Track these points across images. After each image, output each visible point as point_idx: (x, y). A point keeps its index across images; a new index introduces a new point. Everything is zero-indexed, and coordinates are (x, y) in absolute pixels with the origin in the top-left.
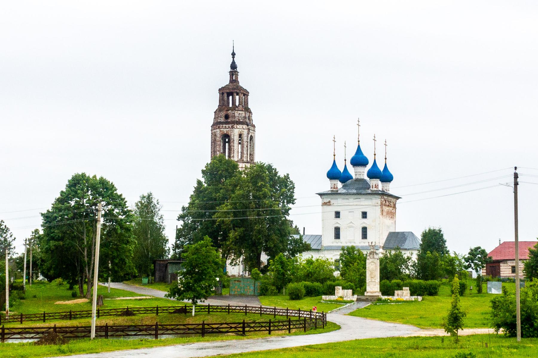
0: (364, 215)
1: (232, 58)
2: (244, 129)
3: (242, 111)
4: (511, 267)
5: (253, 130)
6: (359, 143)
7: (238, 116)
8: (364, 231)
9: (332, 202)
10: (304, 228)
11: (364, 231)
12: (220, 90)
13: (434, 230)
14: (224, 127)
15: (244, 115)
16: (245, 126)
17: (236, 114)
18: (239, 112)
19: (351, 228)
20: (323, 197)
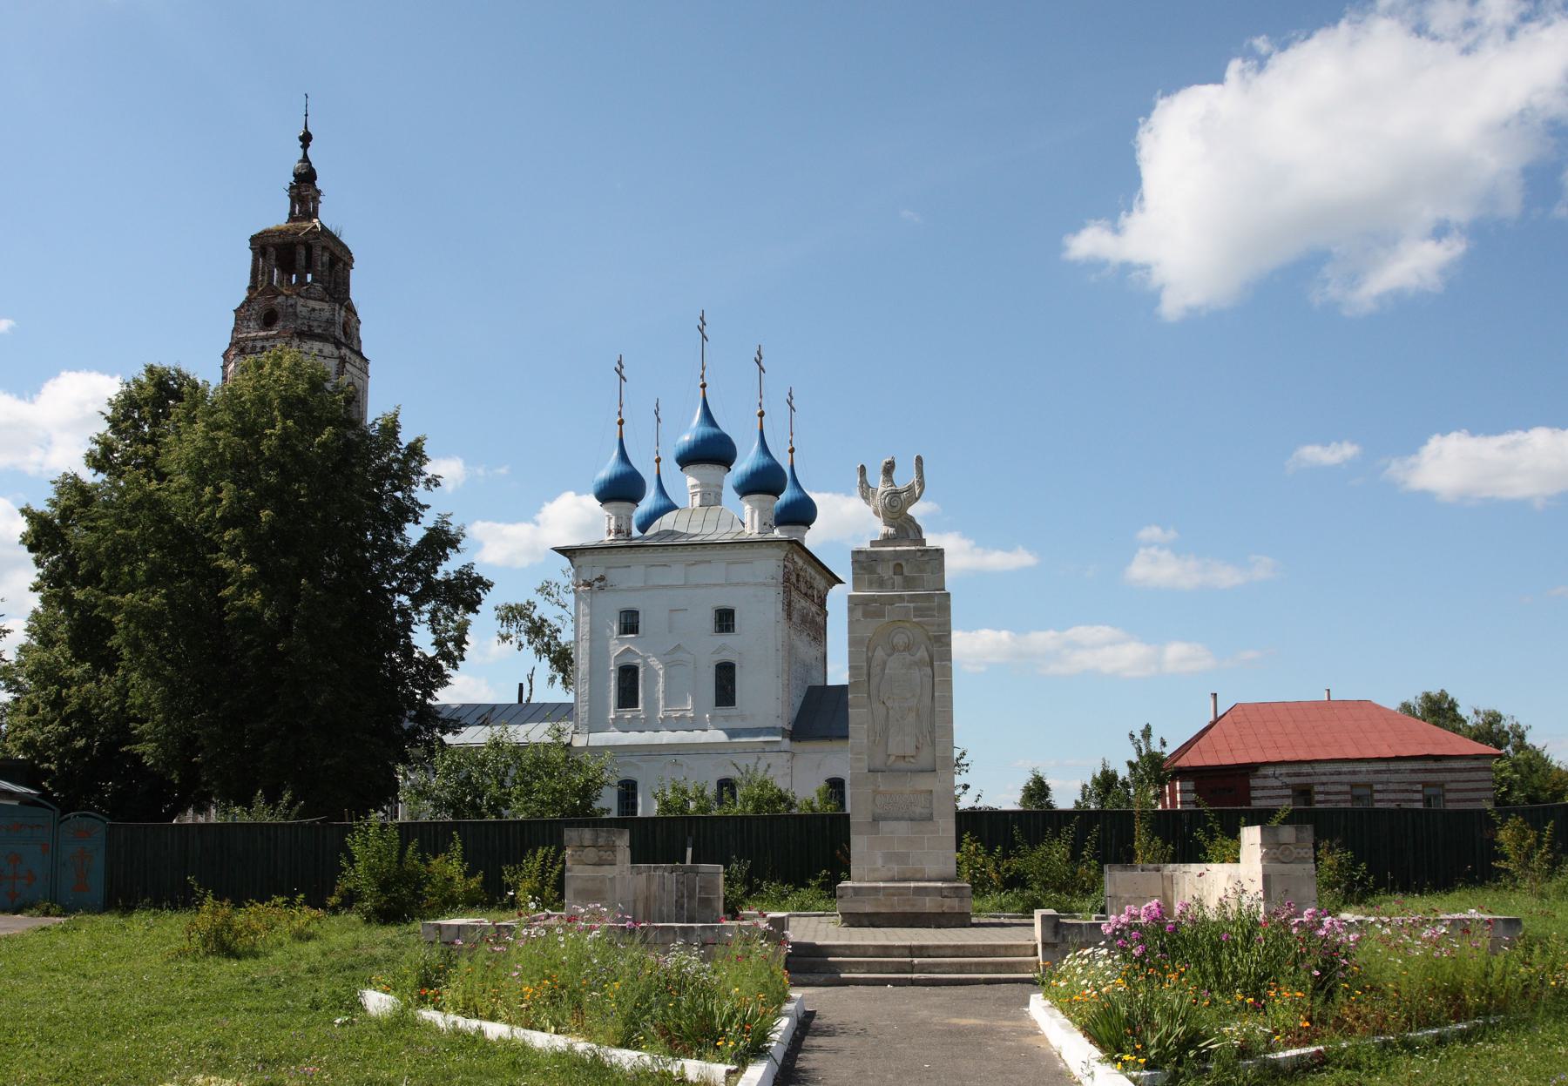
0: (725, 620)
2: (325, 357)
3: (322, 300)
4: (1289, 792)
5: (361, 369)
7: (307, 315)
9: (614, 576)
10: (919, 460)
12: (253, 239)
14: (258, 349)
15: (327, 315)
16: (329, 349)
17: (299, 308)
18: (312, 304)
20: (579, 560)
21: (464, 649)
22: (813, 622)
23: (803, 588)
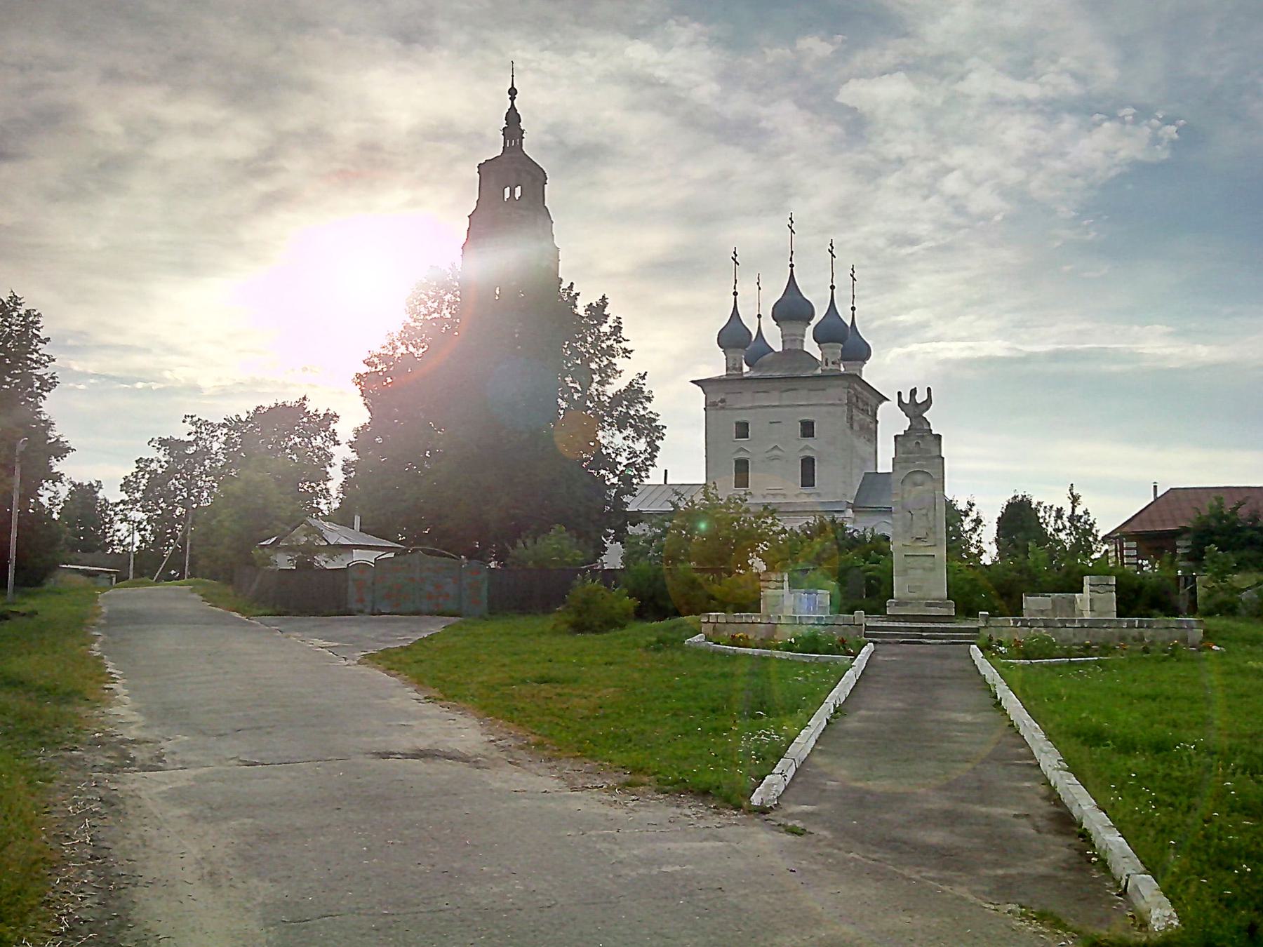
0: (807, 429)
1: (510, 101)
6: (792, 271)
8: (808, 466)
9: (730, 399)
11: (808, 466)
13: (49, 425)
19: (777, 461)
21: (658, 448)
22: (868, 428)
23: (861, 405)
